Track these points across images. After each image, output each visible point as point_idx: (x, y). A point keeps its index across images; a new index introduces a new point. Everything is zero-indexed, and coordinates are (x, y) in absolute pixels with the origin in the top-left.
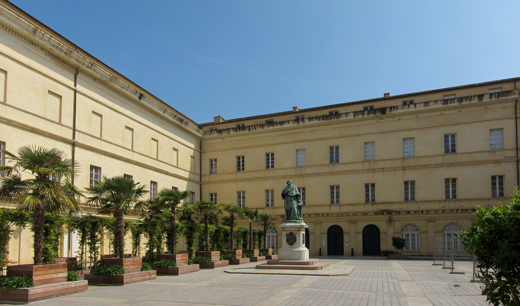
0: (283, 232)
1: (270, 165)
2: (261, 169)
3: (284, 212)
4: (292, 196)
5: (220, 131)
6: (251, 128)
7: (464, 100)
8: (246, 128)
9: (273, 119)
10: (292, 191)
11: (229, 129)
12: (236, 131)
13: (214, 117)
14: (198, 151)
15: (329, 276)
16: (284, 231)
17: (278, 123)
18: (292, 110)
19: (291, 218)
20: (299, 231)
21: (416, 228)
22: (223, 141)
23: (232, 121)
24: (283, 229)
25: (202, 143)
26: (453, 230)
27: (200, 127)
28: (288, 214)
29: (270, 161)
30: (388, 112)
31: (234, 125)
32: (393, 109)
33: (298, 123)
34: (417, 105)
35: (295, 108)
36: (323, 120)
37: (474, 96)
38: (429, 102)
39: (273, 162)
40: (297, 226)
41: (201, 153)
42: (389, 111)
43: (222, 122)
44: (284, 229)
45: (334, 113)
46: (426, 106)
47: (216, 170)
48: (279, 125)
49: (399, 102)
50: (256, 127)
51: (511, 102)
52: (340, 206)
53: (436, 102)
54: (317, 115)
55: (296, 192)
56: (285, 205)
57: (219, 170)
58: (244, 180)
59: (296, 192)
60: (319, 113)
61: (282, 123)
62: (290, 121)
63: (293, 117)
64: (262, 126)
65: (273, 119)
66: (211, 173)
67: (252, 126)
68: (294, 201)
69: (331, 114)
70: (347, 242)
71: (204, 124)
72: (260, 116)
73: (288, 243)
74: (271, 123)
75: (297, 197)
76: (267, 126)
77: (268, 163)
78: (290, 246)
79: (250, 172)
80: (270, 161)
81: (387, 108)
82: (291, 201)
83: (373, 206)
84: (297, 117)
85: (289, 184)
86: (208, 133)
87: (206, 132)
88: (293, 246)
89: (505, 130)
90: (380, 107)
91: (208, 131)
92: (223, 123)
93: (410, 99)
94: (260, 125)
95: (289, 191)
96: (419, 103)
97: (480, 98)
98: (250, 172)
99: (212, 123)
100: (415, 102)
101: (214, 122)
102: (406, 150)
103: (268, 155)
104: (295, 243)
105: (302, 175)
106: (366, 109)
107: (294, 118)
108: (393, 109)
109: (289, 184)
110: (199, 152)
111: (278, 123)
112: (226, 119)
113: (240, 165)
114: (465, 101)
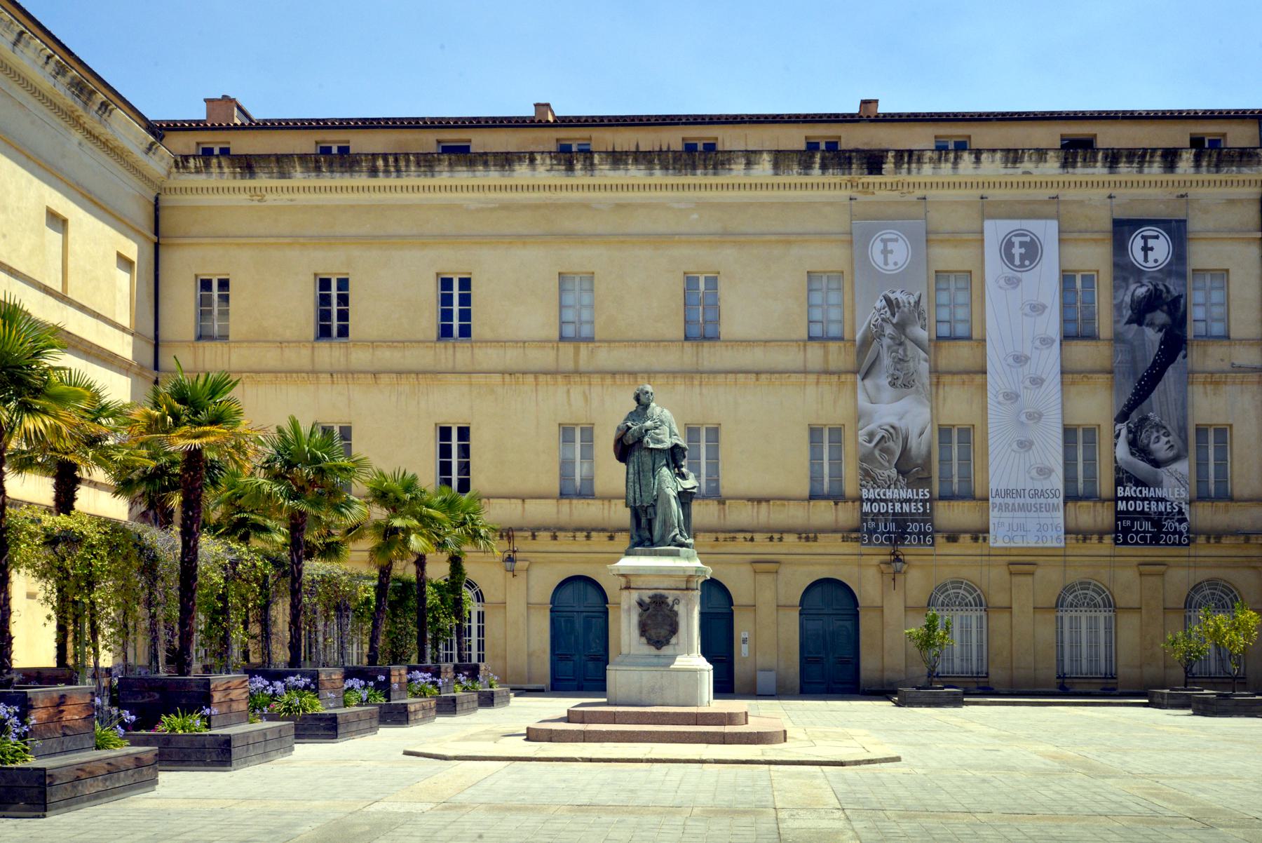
0: (625, 593)
1: (456, 323)
2: (420, 337)
3: (621, 514)
4: (658, 449)
5: (247, 165)
6: (380, 163)
7: (1124, 160)
8: (358, 163)
9: (348, 142)
10: (657, 431)
11: (289, 156)
12: (318, 169)
13: (206, 100)
14: (144, 235)
15: (841, 764)
16: (628, 588)
17: (490, 158)
18: (530, 112)
19: (656, 538)
20: (690, 592)
21: (975, 595)
22: (256, 203)
23: (341, 123)
24: (623, 580)
25: (161, 204)
26: (1088, 604)
27: (159, 130)
28: (643, 521)
29: (456, 308)
30: (888, 166)
31: (305, 143)
32: (906, 159)
33: (570, 168)
34: (984, 156)
35: (542, 107)
36: (665, 167)
37: (1154, 150)
38: (1020, 152)
39: (466, 315)
40: (682, 573)
41: (157, 246)
42: (892, 166)
43: (239, 123)
44: (628, 582)
45: (700, 147)
46: (1009, 165)
47: (227, 327)
48: (495, 165)
49: (921, 138)
50: (402, 164)
51: (683, 185)
52: (722, 506)
53: (1041, 154)
54: (637, 146)
55: (670, 437)
56: (631, 484)
57: (237, 326)
58: (349, 373)
59: (672, 434)
60: (647, 139)
61: (506, 160)
62: (538, 157)
63: (547, 137)
64: (426, 162)
65: (470, 141)
66: (200, 338)
67: (385, 157)
68: (665, 471)
69: (690, 148)
70: (744, 641)
71: (175, 122)
72: (417, 120)
73: (644, 640)
74: (459, 154)
75: (674, 456)
76: (446, 163)
77: (446, 315)
78: (652, 650)
79: (373, 344)
80: (456, 308)
81: (887, 151)
82: (654, 470)
83: (836, 510)
84: (561, 145)
85: (642, 403)
86: (192, 161)
87: (186, 158)
88: (667, 650)
89: (1233, 278)
90: (861, 147)
91: (194, 157)
92: (242, 127)
93: (959, 131)
94: (417, 155)
95: (647, 431)
96: (989, 150)
97: (1169, 159)
98: (373, 344)
99: (198, 122)
100: (975, 144)
101: (205, 118)
102: (817, 314)
103: (446, 284)
104: (673, 640)
105: (577, 372)
106: (812, 147)
107: (678, 146)
108: (906, 159)
109: (642, 403)
110: (148, 238)
111: (490, 158)
112: (258, 114)
113: (329, 312)
114: (1125, 162)
